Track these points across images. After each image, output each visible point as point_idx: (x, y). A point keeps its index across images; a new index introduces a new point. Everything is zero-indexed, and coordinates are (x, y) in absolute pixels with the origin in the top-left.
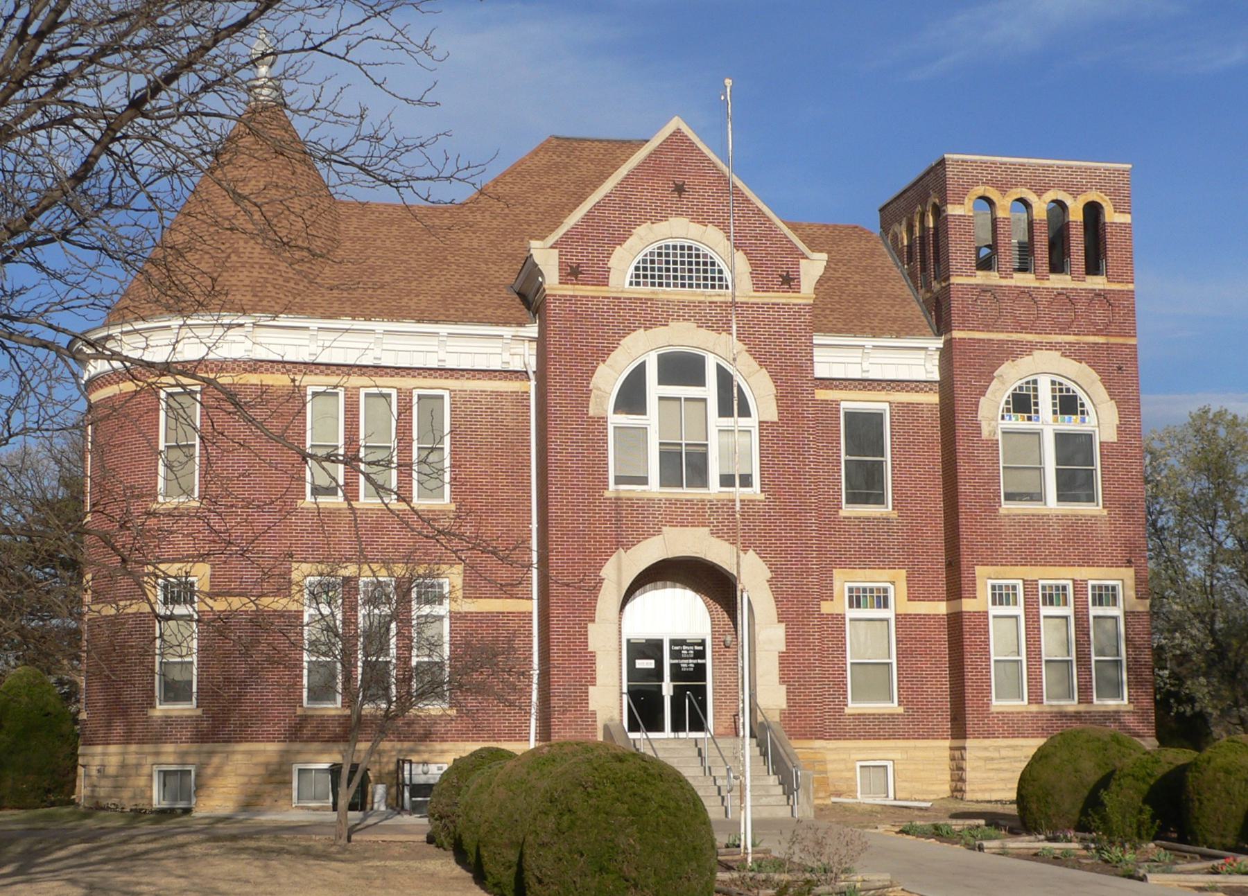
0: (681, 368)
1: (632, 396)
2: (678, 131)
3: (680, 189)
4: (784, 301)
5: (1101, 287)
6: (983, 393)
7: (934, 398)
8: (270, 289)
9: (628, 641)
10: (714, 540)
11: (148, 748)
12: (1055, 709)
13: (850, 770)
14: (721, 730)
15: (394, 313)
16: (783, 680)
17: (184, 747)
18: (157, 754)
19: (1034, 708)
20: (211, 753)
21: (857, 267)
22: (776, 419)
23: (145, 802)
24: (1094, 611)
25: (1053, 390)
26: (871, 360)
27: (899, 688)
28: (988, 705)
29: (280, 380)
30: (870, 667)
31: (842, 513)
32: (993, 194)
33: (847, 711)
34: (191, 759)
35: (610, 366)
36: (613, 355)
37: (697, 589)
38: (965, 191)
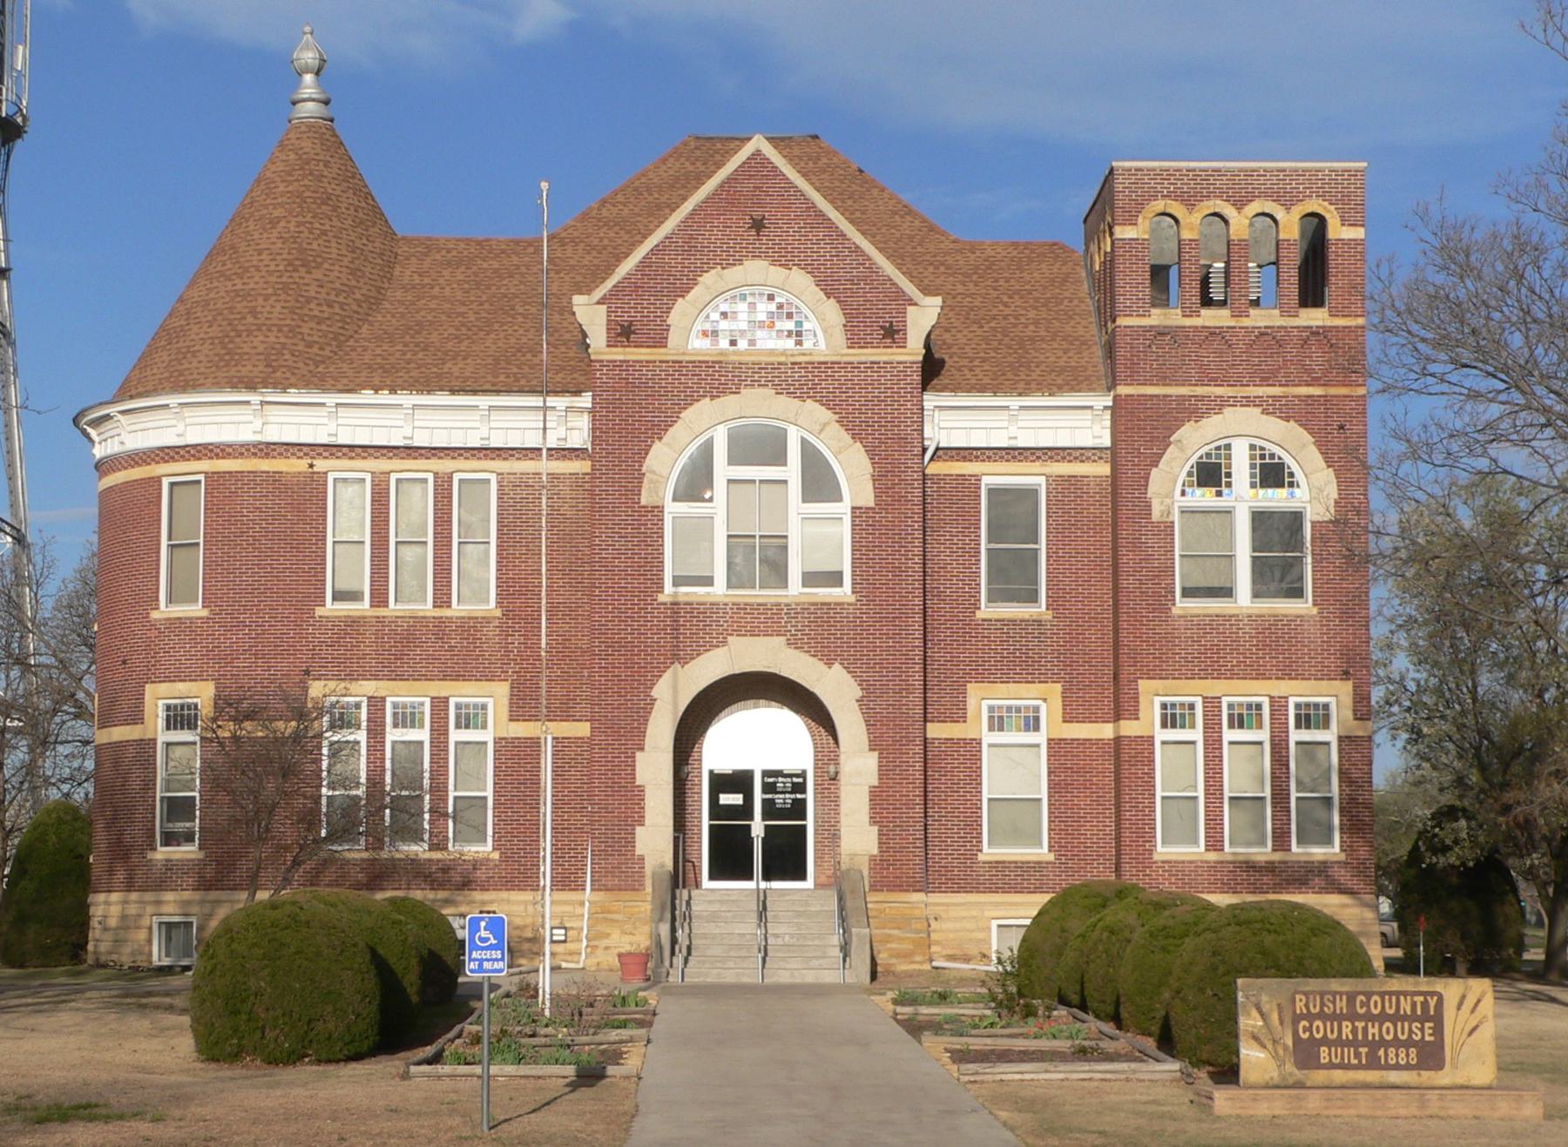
0: (761, 446)
1: (696, 483)
2: (758, 153)
3: (758, 225)
4: (885, 358)
5: (1320, 323)
6: (1155, 464)
7: (1104, 469)
8: (287, 357)
9: (711, 772)
10: (792, 652)
11: (149, 896)
12: (1241, 858)
13: (983, 930)
14: (823, 879)
15: (425, 384)
16: (873, 821)
17: (187, 895)
18: (158, 903)
19: (1213, 856)
20: (218, 902)
21: (1037, 300)
22: (872, 504)
23: (144, 958)
24: (1295, 735)
25: (1252, 457)
26: (1021, 424)
27: (1050, 829)
28: (1151, 852)
29: (298, 465)
30: (1021, 804)
31: (980, 615)
32: (1177, 209)
33: (981, 857)
34: (195, 909)
35: (668, 445)
36: (671, 430)
37: (797, 712)
38: (1139, 207)
